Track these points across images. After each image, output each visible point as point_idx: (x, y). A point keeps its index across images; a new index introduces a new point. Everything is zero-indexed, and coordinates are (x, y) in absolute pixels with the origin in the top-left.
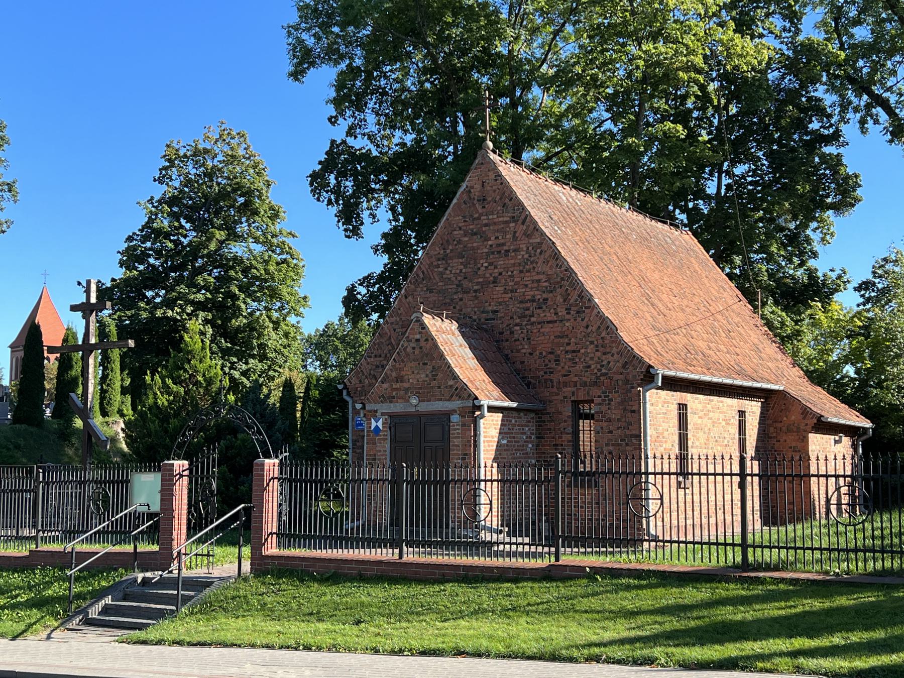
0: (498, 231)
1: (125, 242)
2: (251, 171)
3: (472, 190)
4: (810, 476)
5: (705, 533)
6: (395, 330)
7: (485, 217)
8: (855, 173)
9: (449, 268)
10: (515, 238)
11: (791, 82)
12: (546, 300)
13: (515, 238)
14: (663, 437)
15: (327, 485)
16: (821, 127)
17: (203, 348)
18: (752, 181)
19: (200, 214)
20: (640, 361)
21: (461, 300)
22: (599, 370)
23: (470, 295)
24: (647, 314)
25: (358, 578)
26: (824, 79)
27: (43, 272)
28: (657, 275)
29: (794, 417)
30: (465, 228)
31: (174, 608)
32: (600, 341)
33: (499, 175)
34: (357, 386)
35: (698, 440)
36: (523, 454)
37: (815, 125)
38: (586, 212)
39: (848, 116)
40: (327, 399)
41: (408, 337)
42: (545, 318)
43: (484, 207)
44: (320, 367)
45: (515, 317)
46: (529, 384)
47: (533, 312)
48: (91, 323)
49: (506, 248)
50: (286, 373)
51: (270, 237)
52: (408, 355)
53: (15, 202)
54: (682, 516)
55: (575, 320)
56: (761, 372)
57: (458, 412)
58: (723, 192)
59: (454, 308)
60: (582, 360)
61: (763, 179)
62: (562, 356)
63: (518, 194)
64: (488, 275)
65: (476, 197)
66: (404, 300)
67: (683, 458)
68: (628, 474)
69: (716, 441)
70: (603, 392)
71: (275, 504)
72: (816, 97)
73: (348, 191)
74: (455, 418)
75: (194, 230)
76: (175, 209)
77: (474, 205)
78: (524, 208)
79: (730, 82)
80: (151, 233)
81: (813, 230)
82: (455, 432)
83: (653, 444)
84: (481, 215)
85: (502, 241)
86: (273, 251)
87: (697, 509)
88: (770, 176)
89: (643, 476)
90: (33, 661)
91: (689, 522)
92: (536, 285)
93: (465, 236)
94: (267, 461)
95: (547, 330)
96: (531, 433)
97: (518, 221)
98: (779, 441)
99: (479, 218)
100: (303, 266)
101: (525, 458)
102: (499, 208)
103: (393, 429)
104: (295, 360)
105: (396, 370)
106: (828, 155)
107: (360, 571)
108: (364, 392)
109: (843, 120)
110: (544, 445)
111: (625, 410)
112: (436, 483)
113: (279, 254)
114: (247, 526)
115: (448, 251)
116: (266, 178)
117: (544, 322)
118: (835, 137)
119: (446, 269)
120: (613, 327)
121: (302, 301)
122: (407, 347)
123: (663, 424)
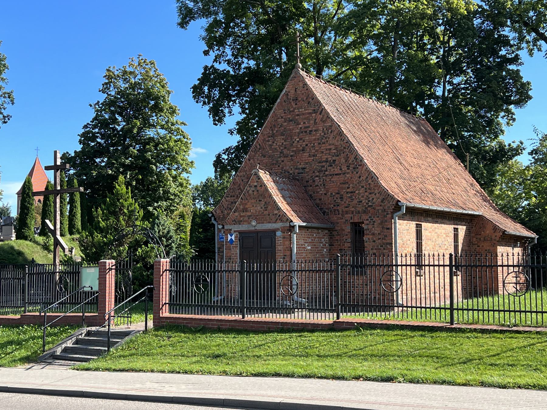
0: (305, 119)
1: (83, 129)
2: (158, 85)
3: (289, 94)
4: (497, 266)
5: (433, 302)
6: (243, 180)
7: (297, 110)
8: (527, 82)
9: (275, 142)
10: (315, 123)
11: (487, 25)
12: (334, 161)
13: (315, 123)
14: (407, 244)
15: (198, 274)
16: (507, 53)
17: (127, 193)
18: (464, 87)
19: (127, 111)
20: (392, 197)
21: (283, 161)
22: (367, 204)
23: (288, 158)
24: (397, 169)
25: (218, 330)
26: (509, 23)
27: (39, 149)
28: (404, 145)
29: (488, 231)
30: (284, 117)
31: (106, 349)
32: (368, 186)
33: (305, 84)
34: (220, 214)
35: (429, 246)
36: (321, 255)
37: (503, 52)
38: (360, 107)
39: (522, 45)
40: (204, 223)
41: (250, 184)
42: (334, 172)
43: (296, 104)
44: (203, 204)
45: (315, 172)
46: (324, 213)
47: (327, 168)
48: (57, 177)
49: (310, 129)
50: (181, 209)
51: (170, 125)
52: (250, 195)
53: (13, 104)
54: (418, 292)
55: (352, 173)
56: (468, 204)
57: (280, 230)
58: (446, 94)
59: (279, 166)
60: (357, 197)
61: (471, 86)
62: (344, 195)
63: (317, 96)
64: (299, 146)
65: (291, 98)
66: (248, 162)
67: (419, 255)
68: (372, 266)
69: (440, 247)
70: (369, 217)
71: (168, 286)
72: (503, 35)
73: (216, 96)
74: (279, 234)
75: (124, 121)
76: (112, 109)
77: (290, 103)
78: (321, 104)
79: (450, 27)
80: (98, 123)
81: (501, 117)
82: (279, 242)
83: (400, 249)
84: (295, 109)
85: (308, 125)
86: (172, 134)
87: (428, 288)
88: (475, 84)
89: (394, 267)
90: (19, 381)
91: (423, 296)
92: (328, 152)
93: (285, 122)
94: (162, 260)
95: (335, 179)
96: (326, 243)
97: (317, 112)
98: (479, 246)
99: (293, 111)
100: (191, 143)
101: (322, 257)
102: (306, 105)
103: (241, 240)
104: (187, 200)
105: (243, 204)
106: (511, 70)
107: (219, 326)
108: (224, 218)
109: (519, 49)
110: (334, 250)
111: (383, 228)
112: (268, 272)
113: (176, 136)
114: (151, 298)
115: (275, 132)
116: (168, 89)
117: (333, 175)
118: (516, 60)
119: (273, 143)
120: (376, 177)
121: (190, 164)
122: (249, 190)
123: (407, 236)
